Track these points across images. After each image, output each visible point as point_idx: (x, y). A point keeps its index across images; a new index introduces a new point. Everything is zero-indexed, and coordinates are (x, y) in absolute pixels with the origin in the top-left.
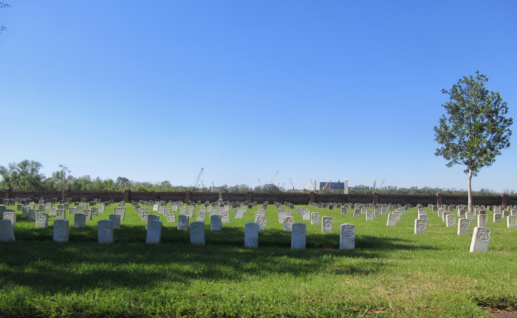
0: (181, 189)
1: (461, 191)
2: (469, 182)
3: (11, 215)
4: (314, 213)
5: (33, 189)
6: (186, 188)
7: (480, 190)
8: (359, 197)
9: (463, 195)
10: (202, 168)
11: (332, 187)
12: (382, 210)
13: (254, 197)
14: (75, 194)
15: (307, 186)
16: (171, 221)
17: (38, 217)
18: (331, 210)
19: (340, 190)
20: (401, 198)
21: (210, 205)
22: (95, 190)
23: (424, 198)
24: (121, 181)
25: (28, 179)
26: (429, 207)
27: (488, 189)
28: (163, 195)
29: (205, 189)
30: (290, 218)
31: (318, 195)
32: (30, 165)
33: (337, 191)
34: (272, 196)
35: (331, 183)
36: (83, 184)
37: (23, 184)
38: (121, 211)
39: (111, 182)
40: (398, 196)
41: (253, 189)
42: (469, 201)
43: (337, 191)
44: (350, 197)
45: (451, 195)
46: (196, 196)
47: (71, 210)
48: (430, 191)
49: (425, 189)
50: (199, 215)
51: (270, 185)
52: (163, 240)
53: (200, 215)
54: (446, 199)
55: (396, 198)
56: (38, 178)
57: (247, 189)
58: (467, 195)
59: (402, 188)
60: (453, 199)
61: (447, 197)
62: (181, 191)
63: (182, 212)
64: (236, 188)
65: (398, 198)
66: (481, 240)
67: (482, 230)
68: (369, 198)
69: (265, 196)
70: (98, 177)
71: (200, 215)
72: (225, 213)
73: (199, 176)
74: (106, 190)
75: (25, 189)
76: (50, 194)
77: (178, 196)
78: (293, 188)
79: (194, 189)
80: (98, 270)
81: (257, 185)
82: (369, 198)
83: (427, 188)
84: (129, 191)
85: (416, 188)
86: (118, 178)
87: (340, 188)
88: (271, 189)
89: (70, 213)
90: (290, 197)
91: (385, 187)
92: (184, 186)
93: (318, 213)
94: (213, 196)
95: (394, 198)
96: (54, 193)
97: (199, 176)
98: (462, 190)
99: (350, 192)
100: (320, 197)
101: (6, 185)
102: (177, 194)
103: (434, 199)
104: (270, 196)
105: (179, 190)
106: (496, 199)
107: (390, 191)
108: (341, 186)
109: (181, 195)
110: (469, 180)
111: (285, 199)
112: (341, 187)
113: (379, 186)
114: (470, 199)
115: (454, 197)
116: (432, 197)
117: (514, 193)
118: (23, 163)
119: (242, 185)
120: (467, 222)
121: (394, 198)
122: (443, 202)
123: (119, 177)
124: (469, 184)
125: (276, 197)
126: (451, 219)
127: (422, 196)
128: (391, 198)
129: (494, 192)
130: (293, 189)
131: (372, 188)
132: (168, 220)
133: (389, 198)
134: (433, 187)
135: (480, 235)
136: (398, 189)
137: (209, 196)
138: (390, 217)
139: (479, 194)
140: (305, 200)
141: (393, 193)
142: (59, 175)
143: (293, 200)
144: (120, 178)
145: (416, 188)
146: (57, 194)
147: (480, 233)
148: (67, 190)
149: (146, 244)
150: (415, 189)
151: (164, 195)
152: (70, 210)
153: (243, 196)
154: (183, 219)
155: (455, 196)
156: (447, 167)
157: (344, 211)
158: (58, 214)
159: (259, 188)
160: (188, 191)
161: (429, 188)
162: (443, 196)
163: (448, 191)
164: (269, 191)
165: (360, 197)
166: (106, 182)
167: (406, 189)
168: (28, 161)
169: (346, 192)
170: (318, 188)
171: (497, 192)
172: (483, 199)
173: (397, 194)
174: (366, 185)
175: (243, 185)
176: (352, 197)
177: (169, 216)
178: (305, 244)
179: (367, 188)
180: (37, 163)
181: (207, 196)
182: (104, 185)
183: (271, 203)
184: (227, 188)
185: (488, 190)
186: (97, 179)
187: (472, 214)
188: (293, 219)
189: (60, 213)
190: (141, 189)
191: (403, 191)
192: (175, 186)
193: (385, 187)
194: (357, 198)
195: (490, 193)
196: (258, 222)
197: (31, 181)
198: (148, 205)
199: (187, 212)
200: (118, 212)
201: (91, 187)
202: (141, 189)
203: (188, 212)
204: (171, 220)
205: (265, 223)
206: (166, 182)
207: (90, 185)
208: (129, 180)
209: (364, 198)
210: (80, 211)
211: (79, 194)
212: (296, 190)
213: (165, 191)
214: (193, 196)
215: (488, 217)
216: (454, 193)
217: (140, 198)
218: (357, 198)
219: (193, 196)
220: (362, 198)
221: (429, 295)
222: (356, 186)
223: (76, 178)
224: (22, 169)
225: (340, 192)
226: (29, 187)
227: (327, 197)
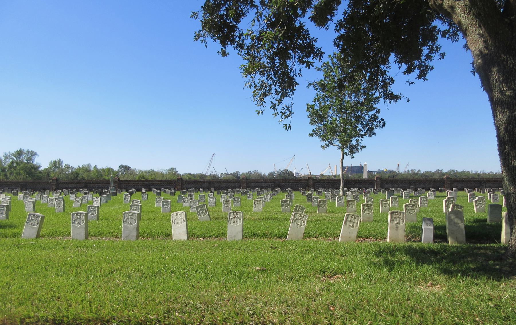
5: (29, 179)
9: (492, 177)
10: (214, 154)
11: (353, 172)
15: (325, 171)
22: (92, 179)
23: (362, 182)
25: (22, 169)
28: (91, 184)
31: (250, 181)
32: (25, 154)
35: (352, 167)
37: (18, 174)
41: (267, 174)
49: (451, 172)
51: (284, 170)
55: (332, 182)
56: (36, 168)
58: (339, 178)
60: (392, 182)
61: (385, 180)
64: (249, 174)
66: (31, 226)
67: (32, 215)
68: (303, 182)
75: (20, 178)
82: (303, 182)
83: (453, 170)
85: (442, 171)
92: (192, 173)
94: (124, 183)
95: (330, 182)
98: (491, 172)
99: (370, 177)
100: (252, 183)
101: (2, 175)
103: (372, 182)
104: (200, 183)
106: (438, 182)
107: (413, 174)
116: (370, 180)
118: (18, 151)
120: (136, 207)
121: (330, 182)
122: (381, 186)
126: (384, 204)
128: (327, 182)
130: (310, 174)
133: (325, 182)
134: (460, 170)
135: (30, 221)
136: (422, 172)
138: (382, 203)
141: (416, 177)
142: (56, 164)
143: (224, 186)
144: (122, 166)
145: (442, 171)
147: (31, 218)
153: (172, 183)
163: (476, 174)
164: (283, 176)
167: (431, 172)
168: (23, 150)
169: (365, 176)
175: (255, 171)
176: (286, 182)
178: (432, 236)
180: (32, 152)
181: (136, 183)
183: (139, 190)
187: (262, 199)
190: (141, 177)
194: (291, 182)
197: (26, 171)
201: (88, 176)
202: (141, 177)
206: (173, 169)
208: (132, 168)
209: (298, 182)
212: (313, 175)
213: (168, 179)
214: (122, 184)
217: (67, 187)
218: (291, 182)
219: (122, 184)
220: (296, 182)
221: (448, 301)
223: (74, 167)
224: (16, 158)
226: (25, 177)
227: (259, 183)
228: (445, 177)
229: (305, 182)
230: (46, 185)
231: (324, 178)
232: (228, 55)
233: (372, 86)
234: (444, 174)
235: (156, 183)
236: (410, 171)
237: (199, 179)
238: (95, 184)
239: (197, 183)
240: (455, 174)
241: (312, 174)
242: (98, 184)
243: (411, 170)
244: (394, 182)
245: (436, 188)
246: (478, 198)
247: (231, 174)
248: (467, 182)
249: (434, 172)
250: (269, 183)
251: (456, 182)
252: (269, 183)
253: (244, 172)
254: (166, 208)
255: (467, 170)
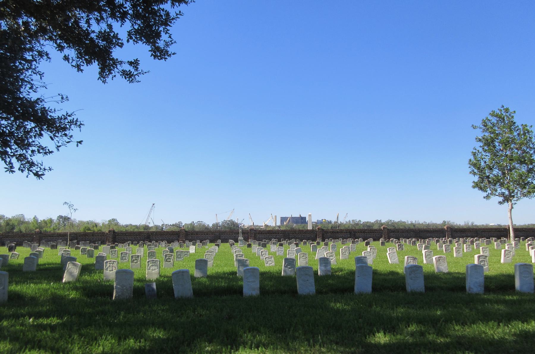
0: (131, 228)
1: (424, 224)
2: (509, 214)
3: (113, 263)
4: (427, 251)
6: (136, 227)
7: (442, 222)
8: (368, 232)
10: (154, 204)
12: (439, 245)
13: (257, 234)
14: (47, 237)
15: (268, 221)
16: (269, 264)
17: (148, 265)
18: (54, 250)
19: (304, 224)
20: (410, 232)
21: (322, 243)
23: (433, 232)
24: (61, 220)
26: (435, 241)
27: (449, 221)
28: (154, 235)
29: (157, 227)
30: (441, 257)
31: (326, 231)
33: (300, 226)
34: (276, 233)
35: (292, 218)
36: (16, 224)
38: (209, 254)
39: (51, 221)
40: (407, 230)
41: (211, 225)
42: (512, 234)
43: (300, 226)
44: (359, 233)
45: (414, 228)
46: (192, 234)
47: (123, 255)
48: (393, 224)
50: (301, 257)
51: (229, 221)
52: (375, 289)
53: (303, 257)
54: (454, 232)
55: (406, 232)
57: (204, 225)
59: (366, 221)
60: (462, 232)
61: (455, 230)
62: (132, 230)
63: (291, 256)
64: (192, 224)
65: (408, 232)
69: (269, 233)
70: (35, 216)
71: (302, 257)
72: (330, 254)
73: (150, 212)
74: (46, 231)
76: (16, 237)
77: (172, 235)
78: (253, 224)
79: (146, 227)
80: (130, 348)
81: (215, 222)
84: (114, 231)
85: (380, 221)
86: (58, 217)
87: (302, 223)
88: (230, 225)
89: (122, 258)
90: (296, 233)
91: (350, 221)
92: (134, 224)
93: (431, 251)
94: (211, 234)
96: (21, 235)
97: (150, 212)
98: (425, 222)
99: (313, 227)
100: (328, 233)
102: (170, 233)
104: (274, 233)
105: (130, 229)
107: (354, 225)
108: (302, 221)
109: (174, 235)
110: (510, 212)
111: (290, 236)
112: (303, 222)
113: (343, 220)
114: (512, 232)
115: (462, 230)
117: (474, 225)
119: (198, 222)
123: (60, 216)
124: (510, 216)
125: (281, 233)
127: (432, 230)
129: (455, 224)
130: (252, 225)
131: (336, 222)
132: (266, 264)
133: (279, 233)
134: (397, 220)
137: (207, 234)
139: (441, 227)
140: (312, 236)
144: (61, 217)
145: (380, 221)
146: (24, 237)
148: (38, 231)
149: (244, 296)
150: (379, 222)
151: (155, 235)
152: (121, 255)
154: (290, 262)
155: (463, 229)
156: (485, 199)
157: (400, 247)
158: (134, 261)
159: (217, 224)
160: (183, 229)
161: (393, 221)
162: (452, 229)
163: (412, 224)
165: (369, 232)
166: (45, 222)
169: (310, 227)
170: (279, 223)
171: (458, 224)
172: (490, 232)
173: (361, 227)
174: (328, 219)
175: (199, 221)
176: (361, 232)
177: (267, 260)
179: (330, 222)
181: (204, 234)
182: (43, 225)
184: (182, 226)
185: (449, 222)
186: (34, 218)
188: (445, 258)
189: (136, 259)
190: (86, 229)
191: (368, 224)
192: (124, 224)
193: (350, 221)
194: (366, 233)
195: (452, 225)
196: (408, 263)
198: (157, 247)
199: (262, 253)
200: (206, 256)
203: (263, 253)
204: (269, 263)
205: (115, 267)
206: (114, 220)
207: (25, 225)
209: (373, 232)
210: (114, 255)
211: (52, 236)
214: (190, 235)
215: (433, 253)
216: (417, 226)
217: (126, 239)
218: (366, 233)
219: (190, 235)
220: (371, 232)
222: (318, 220)
225: (303, 227)
227: (335, 233)
228: (382, 228)
229: (380, 232)
230: (101, 237)
231: (269, 229)
232: (131, 71)
233: (71, 122)
234: (382, 224)
235: (227, 234)
236: (351, 221)
237: (142, 230)
238: (159, 235)
239: (271, 234)
240: (392, 225)
241: (254, 225)
242: (161, 235)
243: (352, 221)
244: (463, 232)
245: (499, 238)
246: (530, 242)
247: (173, 225)
248: (527, 231)
249: (373, 222)
250: (345, 233)
251: (518, 231)
252: (345, 233)
253: (187, 223)
254: (114, 255)
255: (403, 221)
